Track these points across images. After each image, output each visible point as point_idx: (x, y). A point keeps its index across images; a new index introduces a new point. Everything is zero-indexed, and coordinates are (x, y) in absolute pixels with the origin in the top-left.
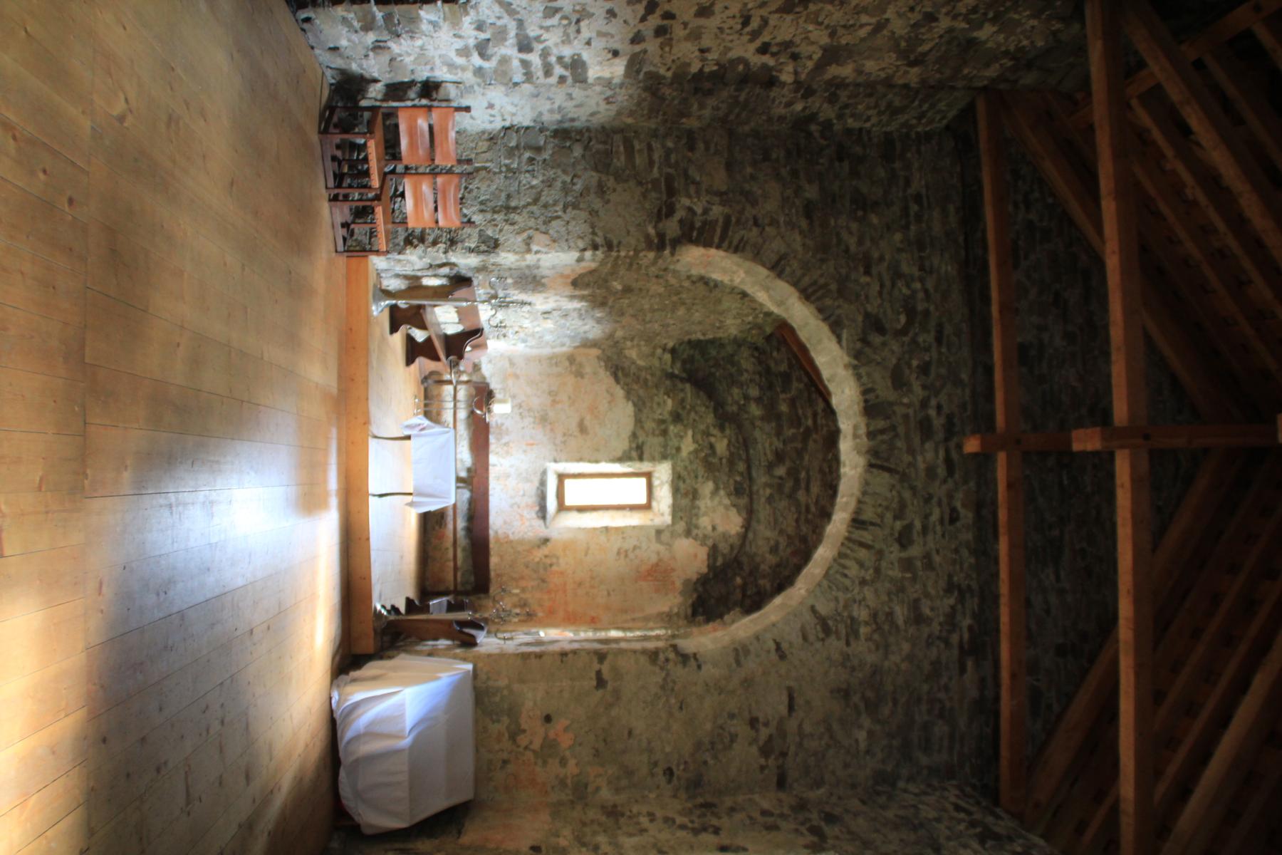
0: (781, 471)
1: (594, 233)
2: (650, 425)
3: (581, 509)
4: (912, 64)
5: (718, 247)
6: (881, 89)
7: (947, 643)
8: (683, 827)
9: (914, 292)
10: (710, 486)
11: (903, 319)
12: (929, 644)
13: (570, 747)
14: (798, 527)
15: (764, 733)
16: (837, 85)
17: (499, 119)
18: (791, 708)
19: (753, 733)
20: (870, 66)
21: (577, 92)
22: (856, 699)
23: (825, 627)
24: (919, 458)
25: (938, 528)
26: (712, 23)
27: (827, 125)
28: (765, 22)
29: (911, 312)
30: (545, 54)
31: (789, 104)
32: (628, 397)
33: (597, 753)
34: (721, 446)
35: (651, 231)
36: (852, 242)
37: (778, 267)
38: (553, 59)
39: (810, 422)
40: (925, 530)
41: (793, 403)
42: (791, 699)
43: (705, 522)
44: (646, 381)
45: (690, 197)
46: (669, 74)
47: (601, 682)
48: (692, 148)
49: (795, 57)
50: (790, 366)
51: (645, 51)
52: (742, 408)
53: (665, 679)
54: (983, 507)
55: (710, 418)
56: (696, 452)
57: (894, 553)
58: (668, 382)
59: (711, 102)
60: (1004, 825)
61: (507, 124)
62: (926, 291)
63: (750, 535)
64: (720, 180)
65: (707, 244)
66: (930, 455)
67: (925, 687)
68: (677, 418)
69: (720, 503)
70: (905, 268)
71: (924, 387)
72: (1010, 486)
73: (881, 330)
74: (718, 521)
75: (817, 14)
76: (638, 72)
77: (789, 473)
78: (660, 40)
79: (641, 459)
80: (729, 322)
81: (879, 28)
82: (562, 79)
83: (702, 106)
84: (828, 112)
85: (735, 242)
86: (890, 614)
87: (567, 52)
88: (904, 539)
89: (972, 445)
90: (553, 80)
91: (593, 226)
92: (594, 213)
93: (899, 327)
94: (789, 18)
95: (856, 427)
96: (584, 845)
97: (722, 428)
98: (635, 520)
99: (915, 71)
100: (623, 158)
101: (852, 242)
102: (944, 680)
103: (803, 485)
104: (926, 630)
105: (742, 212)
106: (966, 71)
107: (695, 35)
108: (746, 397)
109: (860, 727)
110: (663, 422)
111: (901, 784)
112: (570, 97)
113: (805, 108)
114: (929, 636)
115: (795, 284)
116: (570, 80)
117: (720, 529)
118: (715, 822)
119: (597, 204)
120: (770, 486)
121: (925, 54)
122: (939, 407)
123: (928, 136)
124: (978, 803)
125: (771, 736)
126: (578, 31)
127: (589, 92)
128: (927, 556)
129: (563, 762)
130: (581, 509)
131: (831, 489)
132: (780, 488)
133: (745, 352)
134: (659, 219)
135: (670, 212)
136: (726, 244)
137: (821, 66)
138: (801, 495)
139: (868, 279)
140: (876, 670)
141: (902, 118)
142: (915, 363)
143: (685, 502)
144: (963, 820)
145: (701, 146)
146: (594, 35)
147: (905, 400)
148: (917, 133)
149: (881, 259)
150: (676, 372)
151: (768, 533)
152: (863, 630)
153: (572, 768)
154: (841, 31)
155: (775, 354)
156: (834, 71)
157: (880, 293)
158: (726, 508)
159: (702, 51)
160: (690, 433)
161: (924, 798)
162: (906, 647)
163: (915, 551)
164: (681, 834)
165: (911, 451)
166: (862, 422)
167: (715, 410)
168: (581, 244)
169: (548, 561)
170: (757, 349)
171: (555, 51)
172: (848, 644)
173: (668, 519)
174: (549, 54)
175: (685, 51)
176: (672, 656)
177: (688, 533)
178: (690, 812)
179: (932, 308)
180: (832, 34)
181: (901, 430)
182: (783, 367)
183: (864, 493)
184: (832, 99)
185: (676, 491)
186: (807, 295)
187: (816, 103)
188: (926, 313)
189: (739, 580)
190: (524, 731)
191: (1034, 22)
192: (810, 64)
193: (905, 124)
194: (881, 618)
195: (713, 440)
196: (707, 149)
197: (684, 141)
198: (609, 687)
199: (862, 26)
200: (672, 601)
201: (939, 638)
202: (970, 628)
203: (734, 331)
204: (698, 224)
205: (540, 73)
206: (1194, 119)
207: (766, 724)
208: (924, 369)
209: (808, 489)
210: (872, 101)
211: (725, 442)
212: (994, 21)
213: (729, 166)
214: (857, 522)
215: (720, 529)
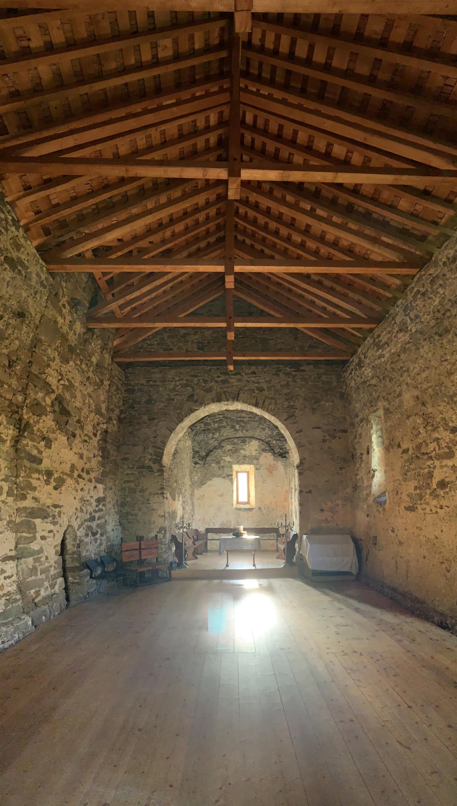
0: (237, 427)
1: (158, 494)
2: (220, 472)
3: (249, 496)
4: (102, 383)
5: (163, 450)
6: (110, 394)
7: (296, 376)
8: (360, 465)
9: (180, 384)
10: (242, 451)
11: (188, 388)
12: (296, 382)
13: (332, 503)
14: (256, 421)
15: (327, 437)
16: (108, 409)
17: (117, 527)
18: (319, 428)
19: (327, 441)
20: (102, 398)
21: (108, 500)
22: (315, 406)
23: (291, 416)
24: (235, 384)
25: (257, 378)
26: (85, 453)
27: (121, 412)
28: (86, 435)
29: (187, 385)
30: (95, 511)
31: (114, 425)
32: (211, 480)
33: (334, 493)
34: (229, 447)
35: (157, 474)
36: (162, 405)
37: (171, 430)
38: (97, 509)
39: (221, 416)
40: (259, 383)
41: (215, 422)
42: (316, 428)
43: (254, 453)
44: (205, 473)
45: (145, 460)
46: (102, 469)
47: (310, 492)
48: (128, 459)
49: (98, 424)
50: (202, 423)
51: (94, 478)
52: (216, 439)
53: (308, 470)
54: (250, 363)
55: (219, 451)
56: (230, 456)
57: (265, 393)
58: (206, 466)
59: (112, 452)
60: (355, 360)
61: (119, 524)
62: (180, 380)
63: (259, 437)
64: (139, 449)
65: (162, 454)
66: (233, 380)
67: (310, 383)
68: (218, 463)
69: (248, 448)
70: (172, 387)
71: (211, 382)
72: (244, 356)
73: (192, 396)
74: (254, 449)
75: (84, 417)
76: (101, 480)
77: (238, 424)
78: (91, 473)
79: (232, 475)
80: (187, 445)
81: (90, 396)
82: (103, 505)
83: (113, 456)
84: (117, 412)
85: (162, 444)
86: (286, 394)
87: (95, 504)
88: (261, 390)
89: (231, 368)
90: (104, 508)
91: (155, 494)
92: (150, 494)
93: (191, 390)
94: (85, 427)
95: (225, 405)
96: (367, 498)
97: (223, 447)
98: (252, 477)
99: (105, 382)
100: (131, 484)
101: (162, 405)
102: (308, 377)
103: (242, 419)
104: (291, 383)
105: (151, 442)
106: (106, 366)
107: (89, 459)
108: (212, 438)
109: (325, 404)
110: (219, 468)
111: (343, 391)
112: (109, 502)
113: (116, 420)
114: (293, 382)
115: (177, 425)
116: (104, 503)
117: (257, 448)
118: (358, 455)
119: (147, 493)
120: (242, 430)
121: (100, 380)
122: (218, 377)
123: (126, 377)
124: (349, 366)
125: (329, 435)
126: (88, 501)
127: (108, 496)
128: (266, 382)
129: (337, 505)
130: (249, 496)
131: (242, 411)
132: (243, 427)
133: (197, 438)
134: (153, 471)
135: (150, 467)
136: (163, 448)
137: (101, 415)
138: (245, 420)
139: (175, 399)
140: (305, 399)
141: (120, 386)
142: (203, 385)
143: (247, 460)
144: (355, 373)
145: (127, 456)
146: (89, 495)
147: (216, 388)
148: (125, 380)
149: (168, 395)
150: (203, 463)
151: (258, 431)
152: (292, 403)
153: (339, 502)
154: (91, 409)
155: (198, 428)
156: (104, 411)
157: (180, 395)
158: (249, 446)
159: (94, 457)
160: (224, 458)
161: (348, 384)
162: (297, 389)
163: (265, 386)
164: (363, 465)
165: (233, 386)
166: (223, 403)
167: (217, 449)
168: (161, 498)
169: (266, 508)
170: (196, 434)
171: (94, 508)
172: (297, 409)
173: (252, 466)
174: (95, 510)
175: (94, 463)
176: (300, 468)
177: (257, 459)
178: (355, 462)
179: (186, 378)
180: (91, 412)
181: (225, 390)
182: (203, 425)
183: (247, 403)
184: (113, 410)
185: (243, 463)
186: (181, 420)
187: (114, 416)
188: (187, 380)
189: (274, 442)
190: (326, 518)
191: (93, 344)
192: (101, 419)
193: (122, 385)
194: (287, 397)
195: (226, 450)
196: (128, 453)
197: (125, 462)
198: (311, 489)
199: (89, 402)
200: (280, 464)
201: (293, 378)
202: (290, 368)
203: (190, 442)
204: (155, 457)
205: (102, 513)
206: (129, 297)
207: (325, 437)
208: (205, 381)
209: (244, 417)
210: (114, 397)
211: (227, 446)
212: (91, 357)
213: (135, 445)
214: (256, 405)
215: (257, 448)
